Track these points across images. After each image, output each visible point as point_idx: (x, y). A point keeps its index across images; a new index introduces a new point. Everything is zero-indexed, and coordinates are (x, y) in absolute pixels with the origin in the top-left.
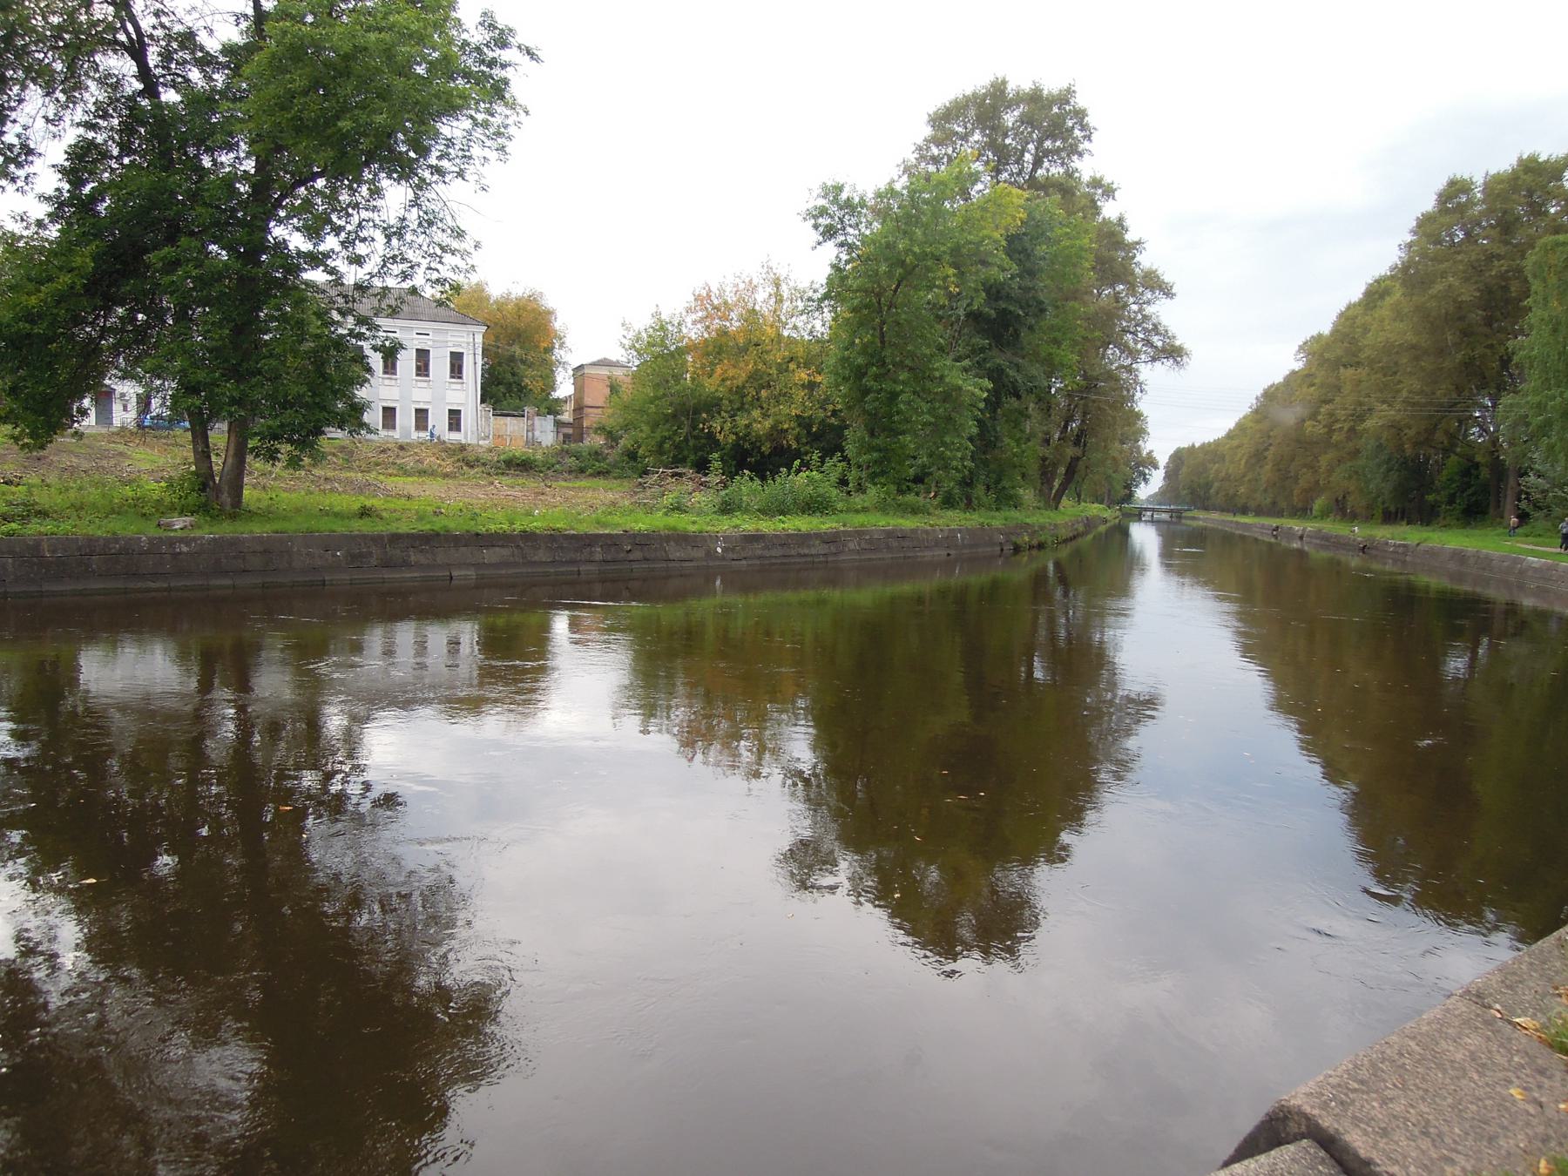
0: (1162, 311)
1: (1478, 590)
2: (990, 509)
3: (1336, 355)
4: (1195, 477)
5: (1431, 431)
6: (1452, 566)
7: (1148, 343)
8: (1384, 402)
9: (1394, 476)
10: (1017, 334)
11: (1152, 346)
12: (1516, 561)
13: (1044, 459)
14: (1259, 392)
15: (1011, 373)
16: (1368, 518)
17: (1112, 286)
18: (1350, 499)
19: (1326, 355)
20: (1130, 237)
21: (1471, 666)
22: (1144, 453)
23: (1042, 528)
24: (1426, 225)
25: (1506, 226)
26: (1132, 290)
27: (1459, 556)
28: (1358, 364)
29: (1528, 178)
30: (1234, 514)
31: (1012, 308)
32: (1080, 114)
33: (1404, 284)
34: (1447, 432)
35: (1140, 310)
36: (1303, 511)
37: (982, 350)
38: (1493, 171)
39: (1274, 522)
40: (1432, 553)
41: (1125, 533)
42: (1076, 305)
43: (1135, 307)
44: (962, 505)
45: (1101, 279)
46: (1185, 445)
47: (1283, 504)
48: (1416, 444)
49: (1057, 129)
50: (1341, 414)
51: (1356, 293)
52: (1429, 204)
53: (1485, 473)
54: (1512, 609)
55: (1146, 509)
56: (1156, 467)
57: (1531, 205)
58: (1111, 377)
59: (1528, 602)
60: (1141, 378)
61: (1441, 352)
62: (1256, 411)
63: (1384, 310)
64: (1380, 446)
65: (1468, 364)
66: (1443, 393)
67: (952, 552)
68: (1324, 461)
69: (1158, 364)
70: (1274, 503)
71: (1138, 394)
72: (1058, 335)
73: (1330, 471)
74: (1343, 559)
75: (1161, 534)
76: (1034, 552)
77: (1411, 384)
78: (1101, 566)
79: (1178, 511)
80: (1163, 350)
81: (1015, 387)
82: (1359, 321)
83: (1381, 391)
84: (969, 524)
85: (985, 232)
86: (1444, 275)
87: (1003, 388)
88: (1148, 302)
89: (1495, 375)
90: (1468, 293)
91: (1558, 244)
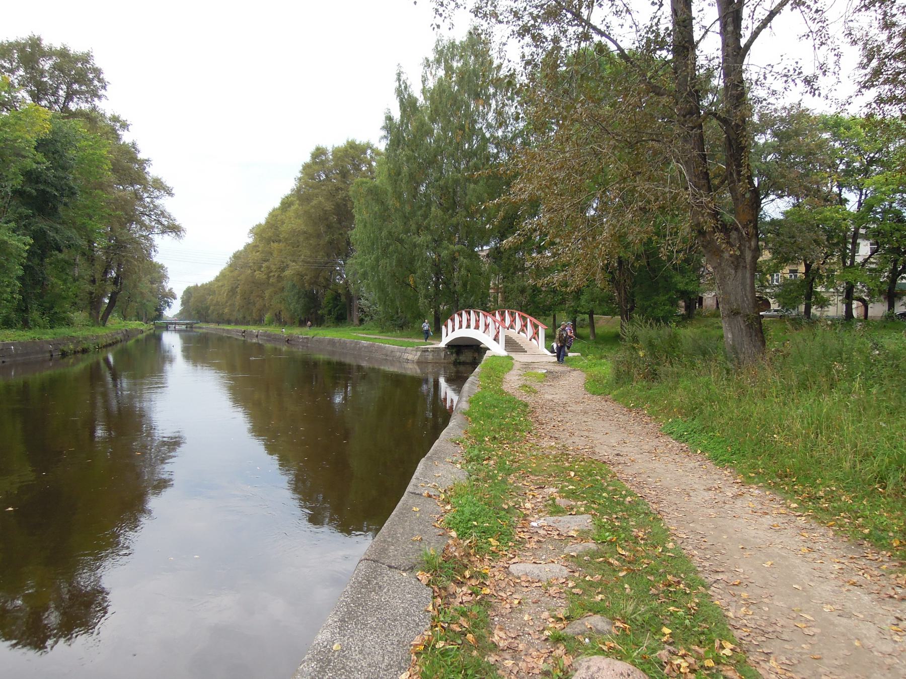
0: (165, 203)
1: (342, 360)
2: (45, 327)
3: (268, 234)
4: (199, 304)
5: (317, 277)
6: (329, 348)
7: (159, 222)
8: (294, 261)
9: (302, 301)
10: (55, 209)
11: (161, 224)
12: (357, 343)
13: (91, 293)
14: (231, 255)
15: (51, 234)
16: (292, 324)
17: (132, 185)
18: (282, 313)
19: (264, 235)
20: (140, 156)
21: (345, 398)
22: (167, 290)
23: (86, 339)
24: (306, 167)
25: (344, 175)
26: (145, 189)
27: (332, 342)
28: (280, 241)
29: (352, 151)
30: (219, 325)
31: (49, 190)
32: (97, 72)
33: (299, 199)
34: (324, 278)
35: (152, 202)
36: (259, 321)
37: (27, 217)
38: (336, 146)
39: (243, 328)
40: (320, 341)
41: (159, 339)
42: (100, 192)
43: (148, 200)
44: (19, 326)
45: (120, 179)
46: (192, 285)
47: (249, 318)
48: (310, 284)
49: (81, 78)
50: (273, 267)
51: (277, 204)
52: (308, 159)
53: (343, 299)
54: (359, 368)
55: (172, 324)
56: (175, 298)
57: (354, 165)
58: (134, 241)
59: (364, 364)
60: (155, 243)
61: (319, 236)
62: (231, 266)
63: (291, 213)
64: (294, 285)
65: (331, 243)
66: (321, 258)
67: (7, 360)
68: (267, 294)
69: (165, 235)
70: (244, 317)
71: (153, 253)
72: (90, 211)
73: (271, 298)
74: (278, 347)
75: (182, 337)
76: (80, 355)
77: (305, 252)
78: (145, 360)
79: (191, 324)
80: (168, 227)
81: (56, 244)
82: (279, 218)
83: (293, 255)
84: (21, 339)
85: (18, 133)
86: (317, 195)
87: (43, 246)
88: (157, 198)
89: (343, 249)
90: (329, 206)
91: (363, 182)
